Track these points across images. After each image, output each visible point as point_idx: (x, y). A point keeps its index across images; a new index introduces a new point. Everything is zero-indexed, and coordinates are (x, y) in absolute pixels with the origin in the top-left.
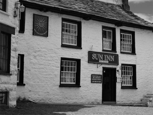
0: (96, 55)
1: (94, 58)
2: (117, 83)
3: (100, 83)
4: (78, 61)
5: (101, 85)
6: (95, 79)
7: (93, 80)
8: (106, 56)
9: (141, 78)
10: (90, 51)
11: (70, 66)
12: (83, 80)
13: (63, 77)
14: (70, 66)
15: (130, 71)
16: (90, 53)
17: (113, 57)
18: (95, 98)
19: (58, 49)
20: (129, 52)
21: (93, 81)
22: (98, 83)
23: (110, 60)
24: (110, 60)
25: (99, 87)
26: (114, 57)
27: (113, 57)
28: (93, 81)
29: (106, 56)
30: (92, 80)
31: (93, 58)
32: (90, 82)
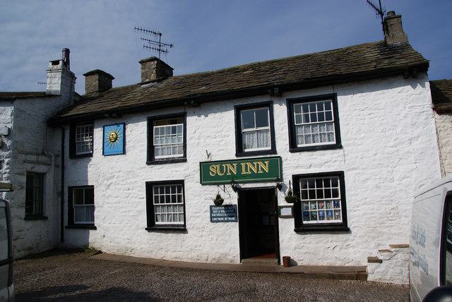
0: (218, 166)
1: (213, 173)
2: (280, 220)
3: (232, 221)
4: (179, 184)
5: (237, 224)
6: (218, 215)
7: (215, 217)
8: (246, 166)
9: (363, 201)
10: (281, 162)
11: (159, 195)
12: (194, 217)
13: (333, 209)
14: (165, 194)
15: (176, 194)
16: (205, 167)
17: (233, 167)
18: (221, 251)
19: (141, 169)
20: (327, 143)
21: (215, 219)
22: (219, 221)
23: (258, 170)
24: (258, 170)
25: (232, 230)
26: (269, 164)
27: (233, 167)
28: (215, 219)
29: (246, 166)
30: (211, 217)
31: (208, 173)
32: (209, 219)
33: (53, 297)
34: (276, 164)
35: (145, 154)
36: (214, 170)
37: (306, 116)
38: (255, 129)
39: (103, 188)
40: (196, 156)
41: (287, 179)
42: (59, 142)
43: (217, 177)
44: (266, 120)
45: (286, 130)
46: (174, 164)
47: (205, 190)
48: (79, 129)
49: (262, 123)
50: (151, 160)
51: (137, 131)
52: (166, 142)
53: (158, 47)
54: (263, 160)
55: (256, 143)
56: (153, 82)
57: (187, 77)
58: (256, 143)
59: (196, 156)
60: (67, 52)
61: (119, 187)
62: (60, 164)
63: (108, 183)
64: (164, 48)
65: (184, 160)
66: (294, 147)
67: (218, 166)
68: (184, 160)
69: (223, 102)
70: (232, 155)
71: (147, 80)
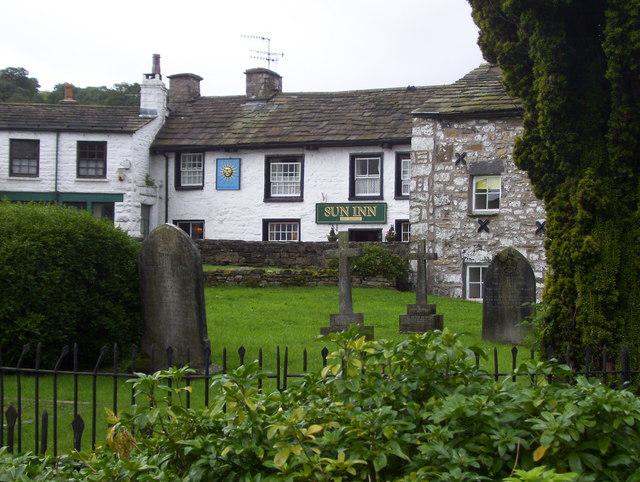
16: (321, 209)
33: (247, 268)
34: (382, 209)
35: (262, 191)
36: (329, 212)
37: (278, 235)
38: (367, 176)
39: (215, 223)
40: (312, 198)
41: (391, 222)
42: (165, 171)
43: (331, 218)
44: (375, 168)
45: (393, 180)
46: (291, 204)
47: (223, 232)
48: (185, 157)
49: (374, 171)
50: (268, 198)
51: (253, 168)
52: (283, 185)
53: (266, 56)
54: (371, 205)
55: (367, 190)
56: (261, 100)
57: (301, 96)
58: (367, 190)
59: (312, 198)
60: (157, 58)
61: (233, 222)
62: (164, 195)
63: (222, 218)
64: (272, 57)
65: (300, 199)
66: (398, 195)
67: (333, 208)
68: (300, 199)
69: (331, 149)
70: (344, 197)
71: (253, 97)
